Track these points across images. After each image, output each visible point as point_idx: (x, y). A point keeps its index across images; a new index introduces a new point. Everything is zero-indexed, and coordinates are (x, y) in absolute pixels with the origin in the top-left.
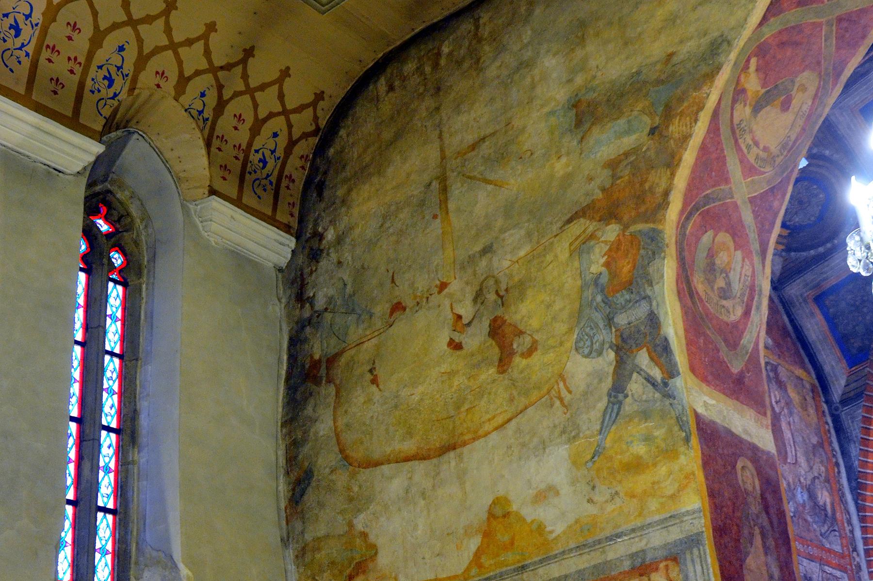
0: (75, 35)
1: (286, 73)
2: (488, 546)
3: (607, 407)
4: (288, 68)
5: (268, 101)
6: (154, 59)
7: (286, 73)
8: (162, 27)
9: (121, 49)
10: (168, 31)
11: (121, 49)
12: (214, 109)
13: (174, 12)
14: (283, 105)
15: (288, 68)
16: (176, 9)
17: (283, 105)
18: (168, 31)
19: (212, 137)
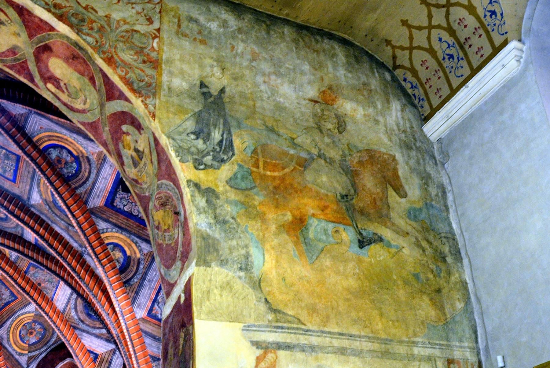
0: (427, 64)
1: (404, 23)
2: (418, 162)
3: (69, 299)
4: (402, 21)
5: (420, 38)
6: (432, 43)
7: (404, 23)
8: (417, 31)
9: (440, 40)
10: (420, 28)
11: (440, 40)
12: (470, 14)
13: (409, 22)
14: (425, 28)
15: (402, 21)
16: (407, 20)
17: (425, 28)
18: (420, 28)
19: (442, 69)
